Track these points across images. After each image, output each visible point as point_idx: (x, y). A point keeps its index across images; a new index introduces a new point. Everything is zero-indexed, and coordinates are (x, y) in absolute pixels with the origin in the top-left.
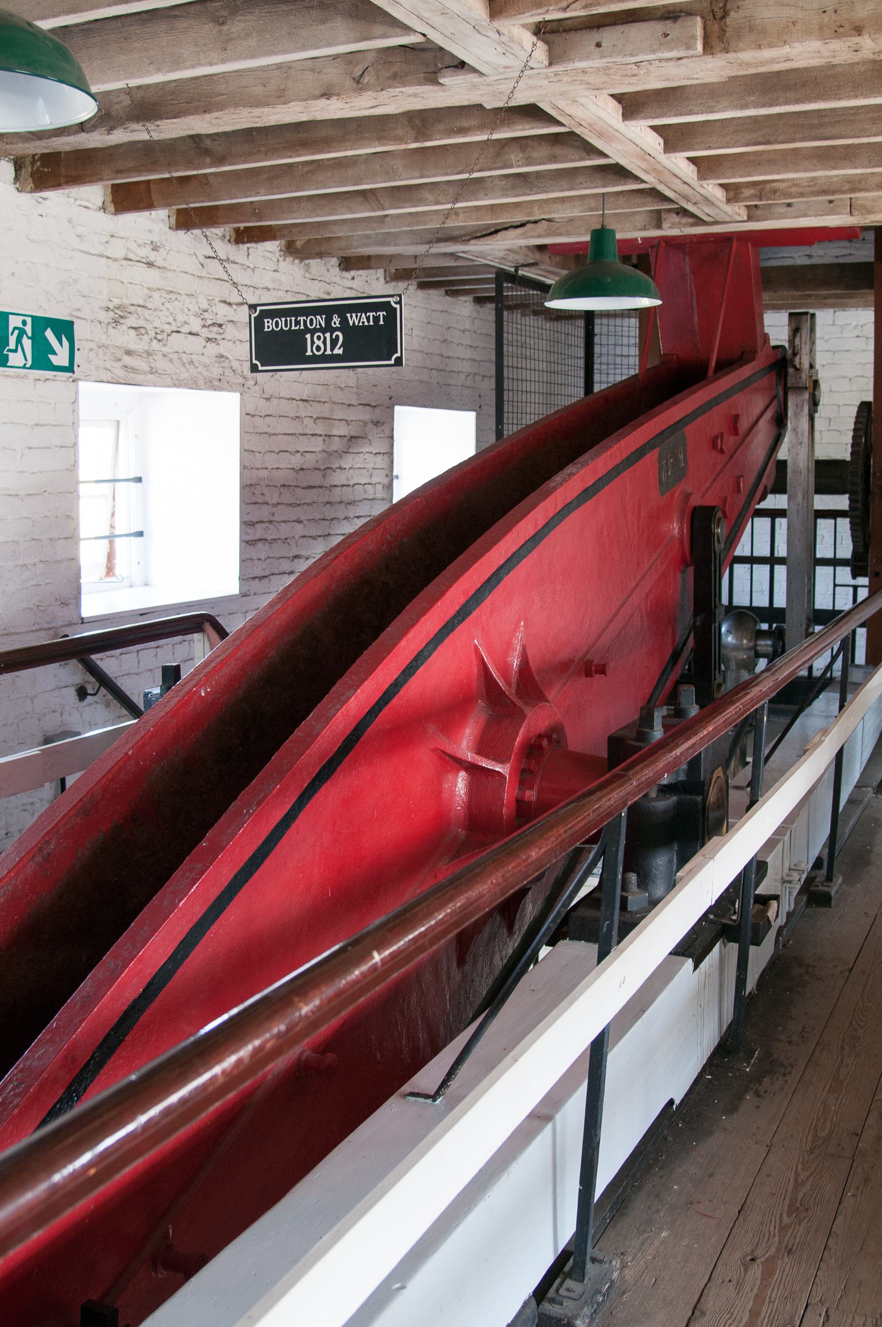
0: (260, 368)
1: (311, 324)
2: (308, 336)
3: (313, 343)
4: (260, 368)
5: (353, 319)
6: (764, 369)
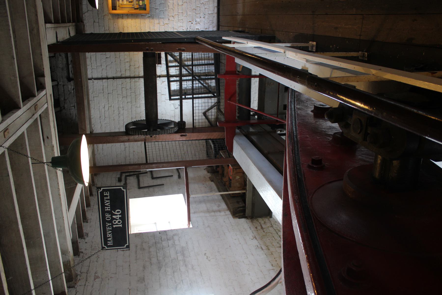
0: (128, 244)
1: (109, 218)
2: (114, 226)
3: (117, 224)
4: (128, 244)
5: (107, 209)
6: (252, 222)
